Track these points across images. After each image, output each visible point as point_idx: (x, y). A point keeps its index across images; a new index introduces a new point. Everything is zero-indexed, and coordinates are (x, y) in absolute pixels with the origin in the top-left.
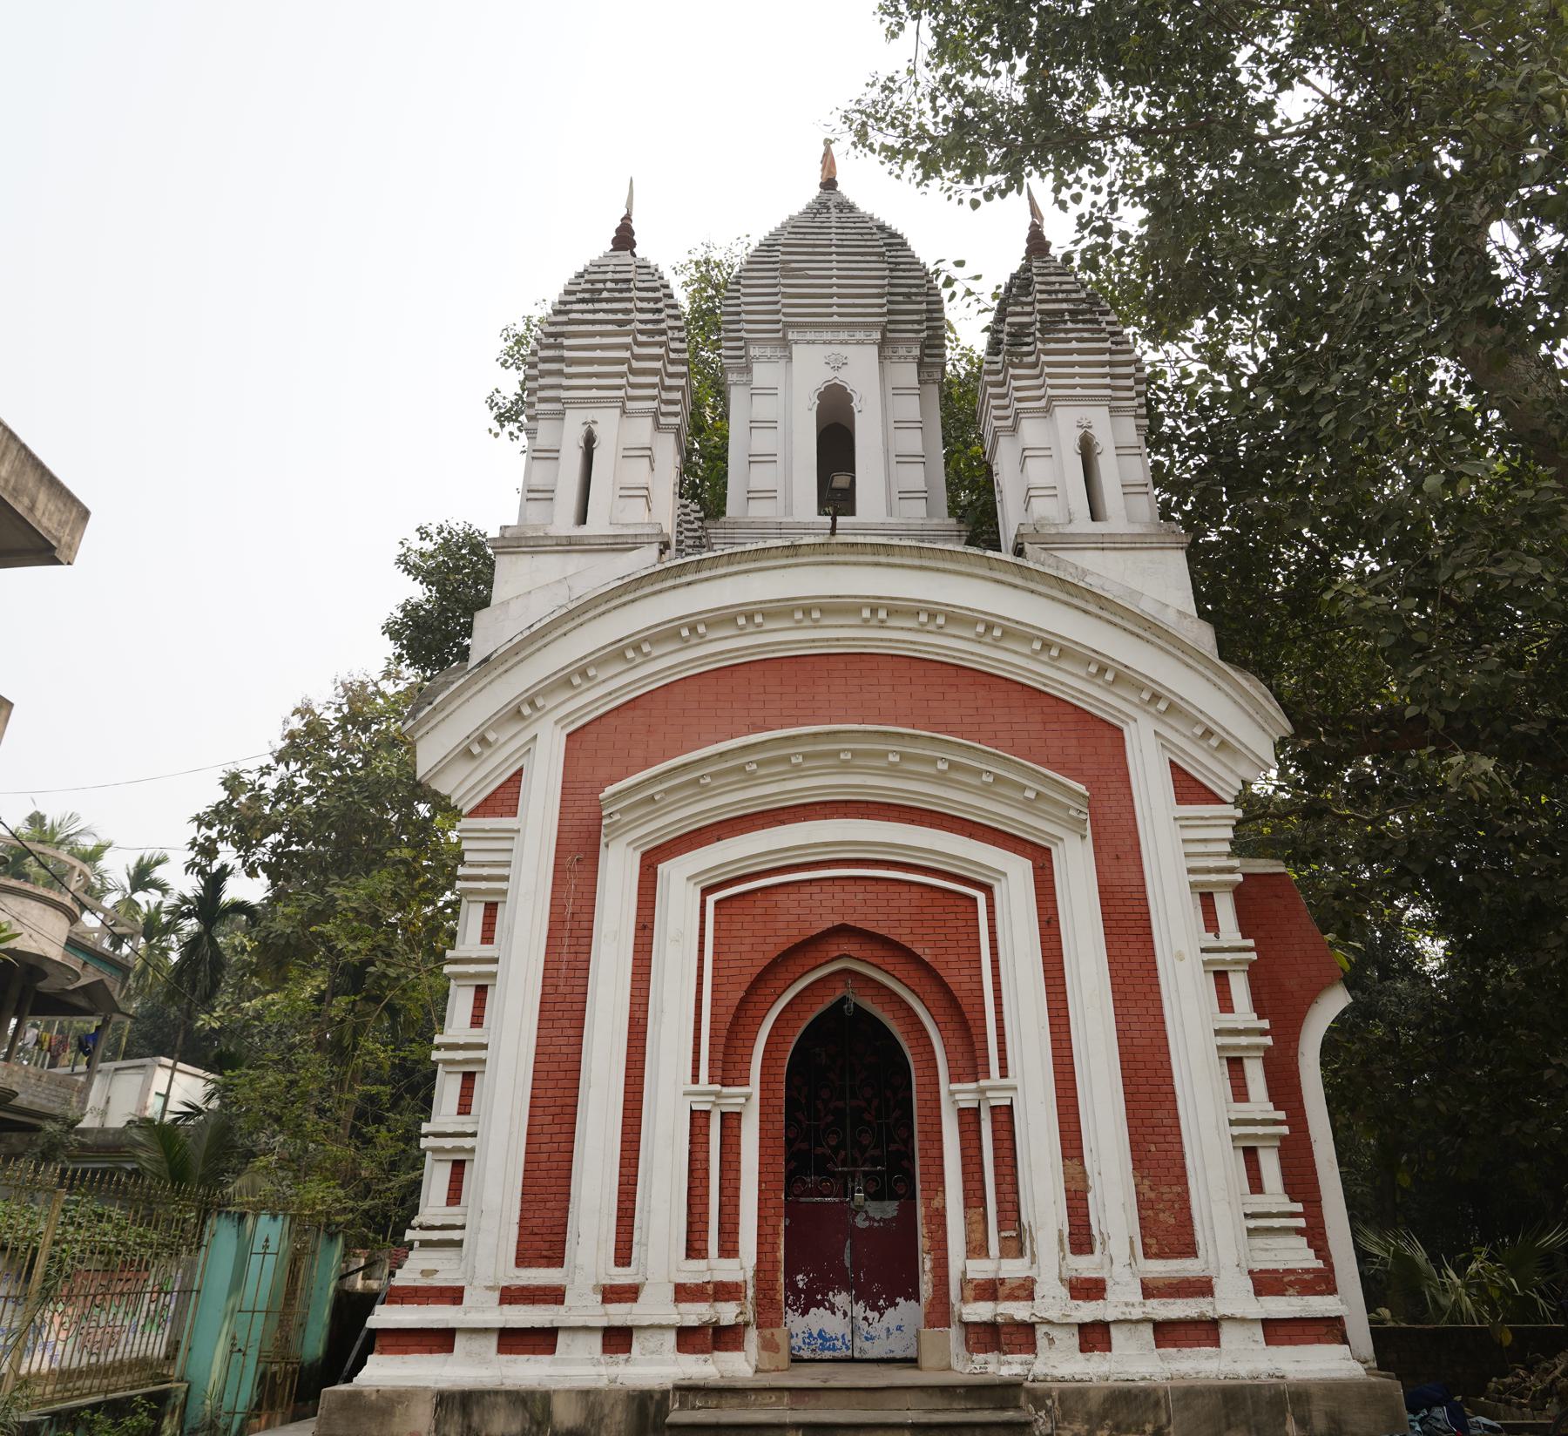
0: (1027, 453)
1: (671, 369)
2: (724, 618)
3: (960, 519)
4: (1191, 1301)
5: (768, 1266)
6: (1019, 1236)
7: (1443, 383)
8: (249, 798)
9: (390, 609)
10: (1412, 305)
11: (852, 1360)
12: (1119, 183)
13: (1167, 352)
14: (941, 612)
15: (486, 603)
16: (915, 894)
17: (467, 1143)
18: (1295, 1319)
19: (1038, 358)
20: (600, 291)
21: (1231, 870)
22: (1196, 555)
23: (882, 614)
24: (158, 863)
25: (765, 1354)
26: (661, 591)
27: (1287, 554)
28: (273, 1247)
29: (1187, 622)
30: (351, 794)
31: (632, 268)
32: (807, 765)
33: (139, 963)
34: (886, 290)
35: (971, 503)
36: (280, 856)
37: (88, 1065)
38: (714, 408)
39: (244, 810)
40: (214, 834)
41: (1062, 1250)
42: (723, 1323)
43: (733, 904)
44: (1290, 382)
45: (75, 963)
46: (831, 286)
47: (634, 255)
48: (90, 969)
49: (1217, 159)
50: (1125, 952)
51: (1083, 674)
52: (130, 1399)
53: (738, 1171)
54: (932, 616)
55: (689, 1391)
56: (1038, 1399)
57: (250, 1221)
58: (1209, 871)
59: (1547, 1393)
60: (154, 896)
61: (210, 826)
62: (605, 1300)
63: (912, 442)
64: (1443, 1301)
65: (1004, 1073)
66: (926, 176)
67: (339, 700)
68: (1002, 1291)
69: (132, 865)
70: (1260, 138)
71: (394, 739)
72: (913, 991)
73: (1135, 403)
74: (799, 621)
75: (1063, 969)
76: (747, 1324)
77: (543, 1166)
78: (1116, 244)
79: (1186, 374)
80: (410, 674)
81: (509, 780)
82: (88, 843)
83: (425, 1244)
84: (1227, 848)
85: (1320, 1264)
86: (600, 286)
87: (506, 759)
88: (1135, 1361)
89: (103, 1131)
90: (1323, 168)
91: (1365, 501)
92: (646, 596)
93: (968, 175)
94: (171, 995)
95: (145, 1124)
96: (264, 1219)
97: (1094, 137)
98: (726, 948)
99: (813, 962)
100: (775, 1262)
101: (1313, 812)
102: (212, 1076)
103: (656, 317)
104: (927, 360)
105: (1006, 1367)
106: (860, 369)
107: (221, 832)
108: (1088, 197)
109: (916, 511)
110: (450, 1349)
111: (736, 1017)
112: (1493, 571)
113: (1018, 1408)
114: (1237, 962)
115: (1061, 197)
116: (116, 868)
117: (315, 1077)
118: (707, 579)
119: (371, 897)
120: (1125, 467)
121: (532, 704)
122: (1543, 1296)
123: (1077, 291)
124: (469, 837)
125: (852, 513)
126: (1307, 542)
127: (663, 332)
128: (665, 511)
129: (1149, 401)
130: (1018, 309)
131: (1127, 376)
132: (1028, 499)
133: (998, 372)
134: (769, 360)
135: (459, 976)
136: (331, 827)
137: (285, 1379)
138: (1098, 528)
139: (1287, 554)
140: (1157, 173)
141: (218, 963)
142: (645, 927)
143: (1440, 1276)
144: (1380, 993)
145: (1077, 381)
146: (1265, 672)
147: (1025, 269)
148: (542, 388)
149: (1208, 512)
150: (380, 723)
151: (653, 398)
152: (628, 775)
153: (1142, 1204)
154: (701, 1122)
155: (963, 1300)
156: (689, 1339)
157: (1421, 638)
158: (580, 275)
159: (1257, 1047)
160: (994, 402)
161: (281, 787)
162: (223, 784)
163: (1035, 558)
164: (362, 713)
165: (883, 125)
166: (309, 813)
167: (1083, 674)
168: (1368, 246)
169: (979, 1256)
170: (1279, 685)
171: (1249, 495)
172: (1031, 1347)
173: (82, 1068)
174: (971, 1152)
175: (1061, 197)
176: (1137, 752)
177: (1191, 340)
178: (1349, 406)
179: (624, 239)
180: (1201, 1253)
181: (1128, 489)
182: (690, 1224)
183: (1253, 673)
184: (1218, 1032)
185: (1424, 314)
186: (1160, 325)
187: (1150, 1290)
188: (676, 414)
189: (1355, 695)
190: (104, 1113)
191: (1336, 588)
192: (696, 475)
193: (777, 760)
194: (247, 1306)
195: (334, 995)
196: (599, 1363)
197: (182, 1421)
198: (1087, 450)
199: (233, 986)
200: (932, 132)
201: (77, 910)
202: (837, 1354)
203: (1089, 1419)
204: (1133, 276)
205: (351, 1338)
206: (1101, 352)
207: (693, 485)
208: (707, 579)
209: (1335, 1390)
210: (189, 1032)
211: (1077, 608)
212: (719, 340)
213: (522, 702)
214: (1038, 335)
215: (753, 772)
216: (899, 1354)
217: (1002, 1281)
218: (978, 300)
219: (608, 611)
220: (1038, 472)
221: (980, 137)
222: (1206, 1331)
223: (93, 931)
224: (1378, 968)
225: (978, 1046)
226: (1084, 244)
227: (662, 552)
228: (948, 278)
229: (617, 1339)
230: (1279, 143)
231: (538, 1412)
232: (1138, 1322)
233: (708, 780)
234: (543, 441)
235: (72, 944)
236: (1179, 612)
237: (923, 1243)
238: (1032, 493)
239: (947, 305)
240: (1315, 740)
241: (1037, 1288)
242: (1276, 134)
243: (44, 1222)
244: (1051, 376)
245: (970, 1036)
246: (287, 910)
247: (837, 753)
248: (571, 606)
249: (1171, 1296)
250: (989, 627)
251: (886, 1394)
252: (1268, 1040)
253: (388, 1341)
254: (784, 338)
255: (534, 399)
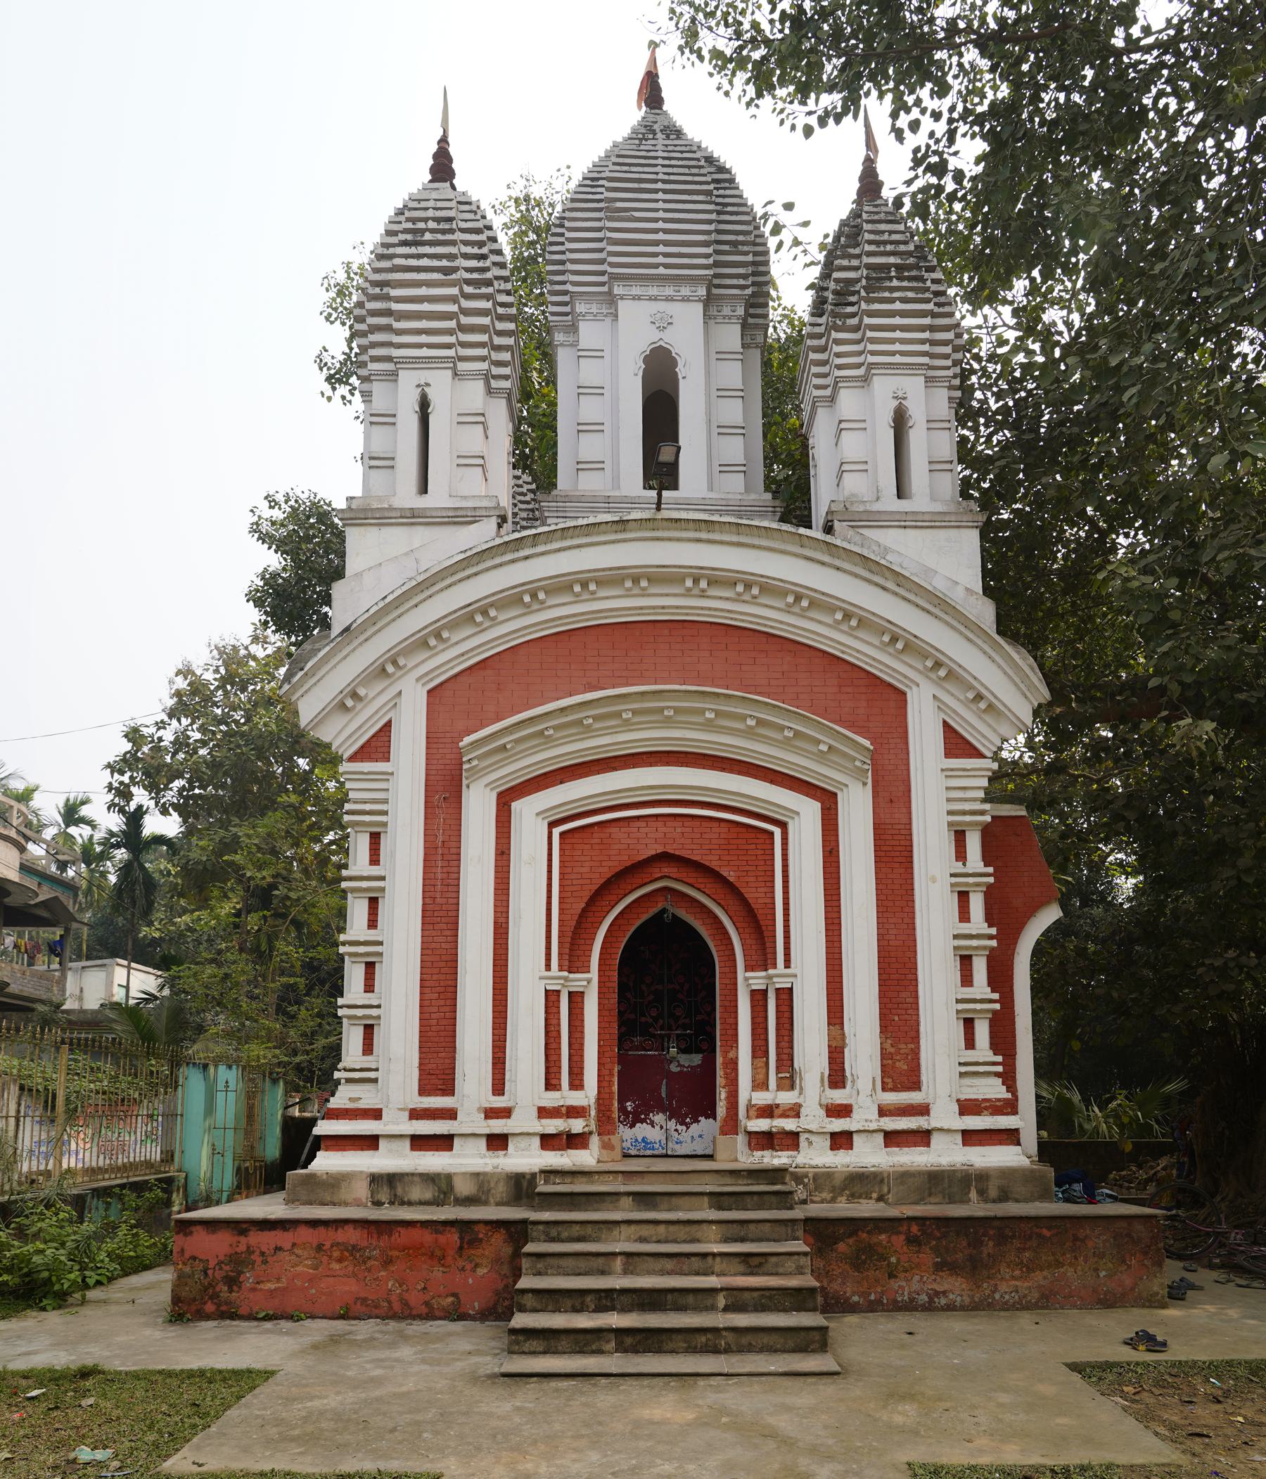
0: (843, 425)
1: (500, 326)
2: (562, 586)
3: (776, 494)
4: (913, 1119)
5: (607, 1096)
6: (792, 1077)
7: (1246, 356)
8: (151, 749)
9: (250, 577)
10: (1236, 266)
11: (667, 1156)
12: (960, 107)
13: (985, 317)
14: (756, 583)
15: (339, 574)
16: (724, 828)
17: (374, 1012)
18: (986, 1130)
19: (861, 320)
20: (423, 231)
21: (982, 813)
22: (988, 531)
23: (703, 584)
24: (83, 803)
25: (605, 1152)
26: (501, 565)
27: (1069, 532)
28: (232, 1086)
29: (973, 599)
30: (239, 746)
31: (453, 204)
32: (636, 720)
33: (84, 884)
34: (713, 237)
35: (787, 478)
36: (187, 798)
37: (60, 964)
38: (541, 372)
39: (149, 759)
40: (126, 778)
41: (823, 1085)
42: (574, 1131)
43: (574, 835)
44: (1101, 352)
45: (31, 883)
46: (656, 231)
47: (454, 188)
48: (45, 888)
49: (1065, 77)
50: (890, 876)
51: (877, 643)
52: (146, 1182)
53: (583, 1032)
54: (748, 586)
55: (549, 1173)
56: (798, 1178)
57: (212, 1069)
58: (964, 813)
59: (1149, 1180)
60: (86, 831)
61: (122, 773)
62: (487, 1117)
63: (733, 412)
64: (1086, 1126)
65: (787, 964)
66: (759, 95)
67: (215, 663)
68: (777, 1112)
69: (61, 805)
70: (1118, 53)
71: (270, 698)
72: (719, 904)
73: (950, 373)
74: (629, 589)
75: (839, 888)
76: (591, 1133)
77: (433, 1028)
78: (950, 186)
79: (1002, 342)
80: (276, 640)
81: (381, 730)
82: (18, 785)
83: (348, 1081)
84: (981, 794)
85: (1009, 1096)
86: (421, 225)
87: (376, 712)
88: (869, 1155)
89: (82, 1011)
90: (1176, 93)
91: (1147, 481)
92: (487, 570)
93: (803, 91)
94: (116, 908)
95: (116, 1006)
96: (222, 1068)
97: (939, 46)
98: (569, 870)
99: (640, 881)
100: (611, 1093)
101: (1055, 769)
102: (160, 973)
103: (481, 264)
104: (751, 320)
105: (778, 1159)
106: (686, 330)
107: (131, 778)
108: (927, 123)
109: (734, 486)
110: (450, 1148)
111: (579, 922)
112: (1253, 552)
113: (784, 1183)
114: (978, 885)
115: (899, 124)
116: (48, 806)
117: (243, 972)
118: (543, 554)
119: (269, 835)
120: (932, 444)
121: (395, 663)
122: (1158, 1122)
123: (905, 243)
124: (357, 780)
125: (676, 487)
126: (1090, 521)
127: (488, 283)
128: (500, 483)
129: (963, 370)
130: (845, 262)
131: (945, 343)
132: (840, 474)
133: (820, 336)
134: (596, 317)
135: (354, 890)
136: (226, 774)
137: (255, 1172)
138: (904, 505)
139: (1069, 532)
140: (1000, 96)
141: (150, 885)
142: (503, 853)
143: (1087, 1110)
144: (1079, 917)
145: (897, 347)
146: (1032, 644)
147: (856, 214)
148: (374, 345)
149: (1004, 491)
150: (256, 684)
151: (483, 359)
152: (482, 727)
153: (884, 1055)
154: (553, 998)
155: (748, 1117)
156: (548, 1141)
157: (1175, 615)
158: (400, 212)
159: (984, 948)
160: (815, 370)
161: (177, 739)
162: (126, 736)
163: (843, 536)
164: (239, 676)
165: (713, 23)
166: (205, 762)
167: (877, 643)
168: (1202, 193)
169: (762, 1089)
170: (1042, 656)
171: (1045, 474)
172: (796, 1147)
173: (55, 966)
174: (759, 1020)
175: (899, 124)
176: (916, 714)
177: (1011, 303)
178: (1154, 379)
179: (442, 168)
180: (924, 1088)
181: (935, 466)
182: (547, 1068)
183: (1023, 645)
184: (956, 937)
185: (1245, 276)
186: (982, 286)
187: (883, 1112)
188: (506, 377)
189: (1107, 666)
190: (81, 999)
191: (1110, 568)
192: (526, 445)
193: (610, 717)
194: (220, 1124)
195: (249, 912)
196: (485, 1156)
197: (186, 1196)
198: (900, 422)
199: (164, 906)
200: (768, 33)
201: (23, 841)
202: (656, 1152)
203: (833, 1189)
204: (961, 227)
205: (300, 1142)
206: (923, 314)
207: (523, 456)
208: (543, 554)
209: (1007, 1174)
210: (135, 940)
211: (877, 585)
212: (542, 294)
213: (386, 661)
214: (863, 293)
215: (589, 726)
216: (700, 1153)
217: (778, 1106)
218: (805, 251)
219: (454, 584)
220: (852, 445)
221: (820, 41)
222: (922, 1137)
223: (40, 858)
224: (1085, 894)
225: (768, 945)
226: (919, 183)
227: (500, 526)
228: (776, 223)
229: (498, 1142)
230: (1136, 56)
231: (444, 1186)
232: (873, 1131)
233: (551, 732)
234: (379, 404)
235: (25, 868)
236: (967, 589)
237: (720, 1081)
238: (845, 467)
239: (773, 257)
240: (1058, 721)
241: (802, 1110)
242: (1133, 45)
243: (56, 1072)
244: (873, 341)
245: (763, 938)
246: (201, 843)
247: (661, 710)
248: (420, 579)
249: (899, 1115)
250: (798, 598)
251: (691, 1175)
252: (994, 943)
253: (329, 1143)
254: (610, 293)
255: (365, 358)
